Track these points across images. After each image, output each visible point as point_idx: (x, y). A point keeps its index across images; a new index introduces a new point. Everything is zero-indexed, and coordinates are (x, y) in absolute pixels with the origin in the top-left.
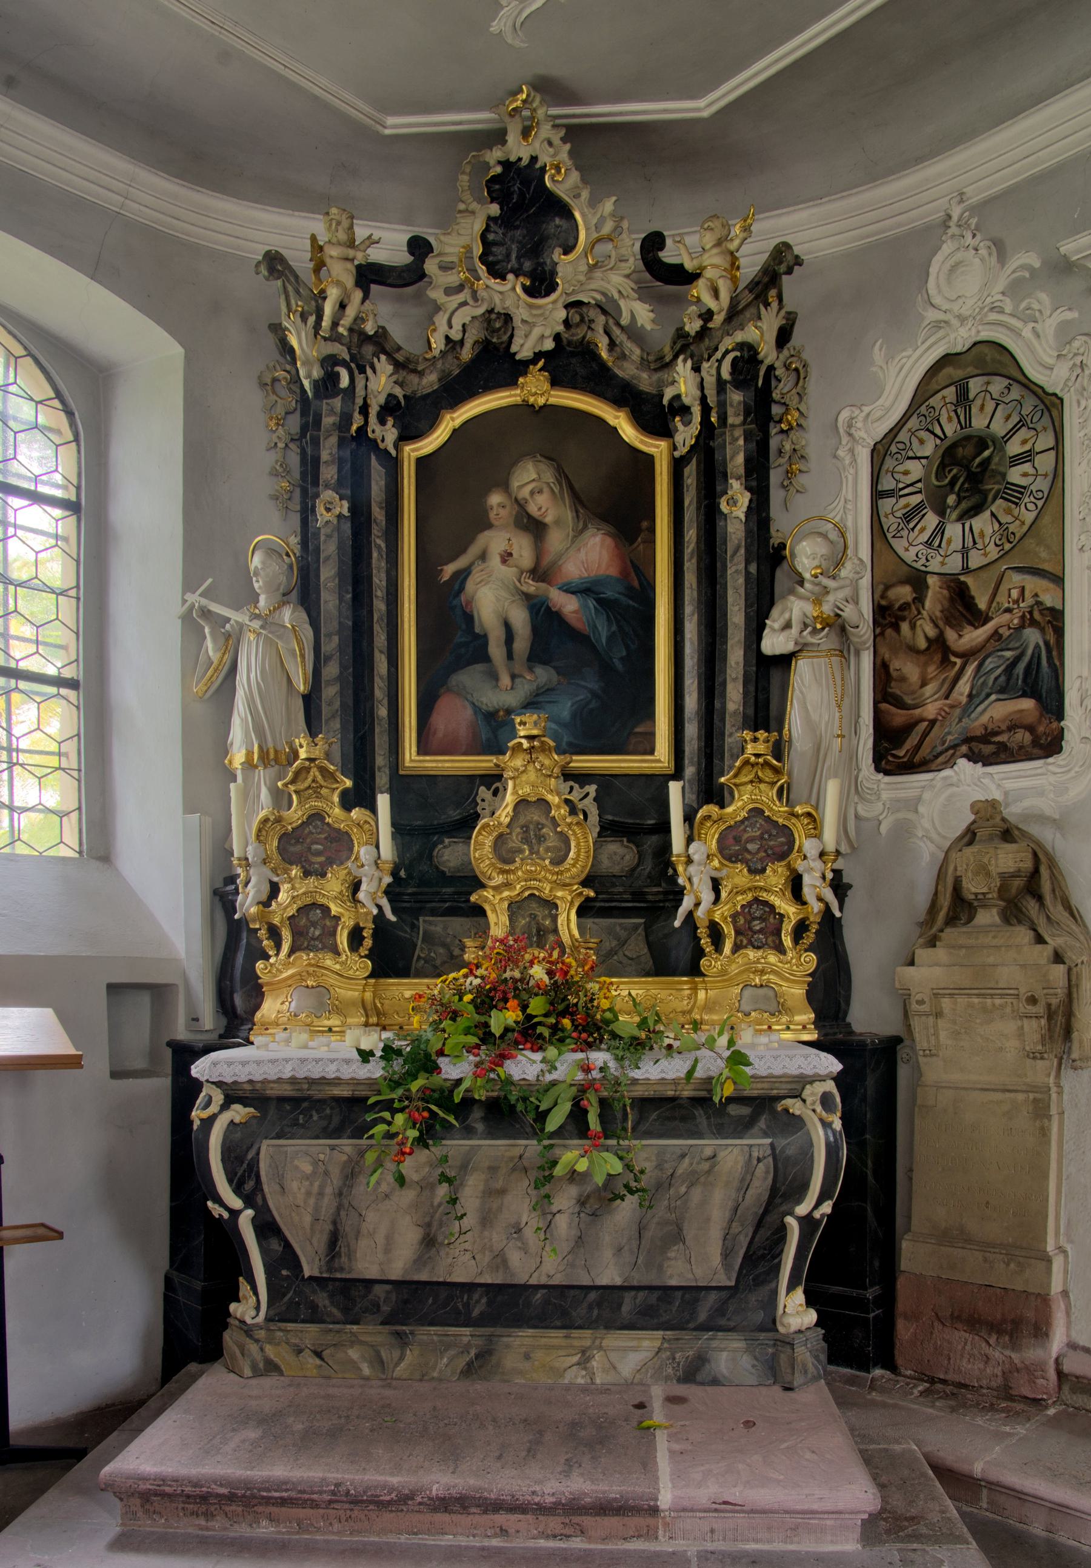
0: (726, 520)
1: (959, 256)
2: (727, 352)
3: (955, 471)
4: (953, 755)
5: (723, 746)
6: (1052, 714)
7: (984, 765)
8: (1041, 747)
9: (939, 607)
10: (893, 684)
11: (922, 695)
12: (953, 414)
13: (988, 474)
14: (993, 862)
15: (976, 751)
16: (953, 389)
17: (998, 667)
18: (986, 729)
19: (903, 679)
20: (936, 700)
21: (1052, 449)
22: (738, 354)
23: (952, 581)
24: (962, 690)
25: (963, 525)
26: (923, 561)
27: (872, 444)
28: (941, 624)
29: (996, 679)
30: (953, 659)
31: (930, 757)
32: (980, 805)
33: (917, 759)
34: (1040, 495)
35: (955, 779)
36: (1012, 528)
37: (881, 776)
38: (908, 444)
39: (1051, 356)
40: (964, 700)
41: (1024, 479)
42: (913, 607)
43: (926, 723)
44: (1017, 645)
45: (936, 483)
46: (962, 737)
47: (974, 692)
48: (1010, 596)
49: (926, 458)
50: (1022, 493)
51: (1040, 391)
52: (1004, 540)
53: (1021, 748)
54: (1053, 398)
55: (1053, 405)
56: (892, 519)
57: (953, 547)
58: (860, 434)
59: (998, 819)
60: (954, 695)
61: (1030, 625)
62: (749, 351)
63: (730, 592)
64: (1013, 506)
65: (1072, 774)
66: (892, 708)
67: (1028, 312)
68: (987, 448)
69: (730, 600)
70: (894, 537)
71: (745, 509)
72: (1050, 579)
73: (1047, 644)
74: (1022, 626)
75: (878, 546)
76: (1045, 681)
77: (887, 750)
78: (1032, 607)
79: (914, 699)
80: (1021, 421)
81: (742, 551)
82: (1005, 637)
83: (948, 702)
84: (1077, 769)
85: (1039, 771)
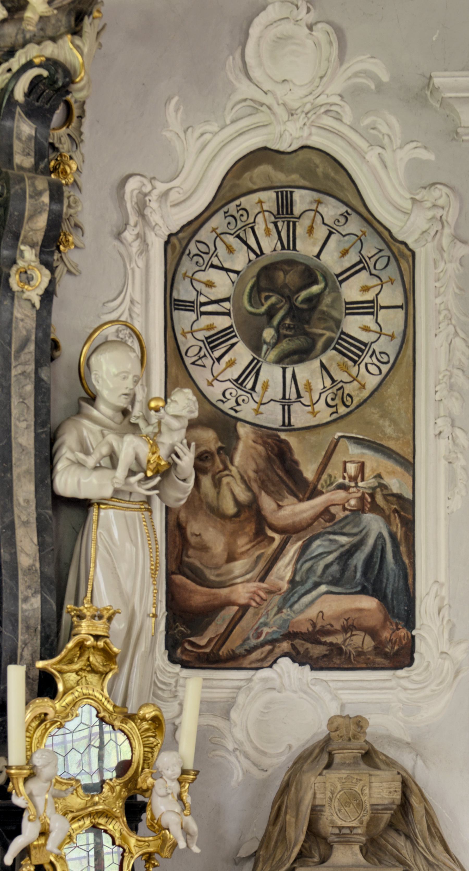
0: (13, 298)
1: (287, 28)
2: (29, 65)
3: (273, 300)
4: (271, 652)
5: (15, 616)
6: (399, 618)
7: (312, 669)
8: (386, 655)
9: (253, 466)
10: (191, 552)
11: (231, 572)
12: (271, 226)
13: (316, 315)
14: (367, 791)
15: (302, 650)
16: (272, 194)
17: (330, 553)
18: (314, 625)
19: (204, 548)
20: (248, 581)
21: (401, 307)
22: (45, 73)
23: (269, 436)
24: (281, 573)
25: (284, 370)
26: (232, 403)
27: (167, 233)
28: (255, 486)
29: (327, 567)
30: (270, 533)
31: (242, 651)
32: (340, 720)
33: (223, 651)
34: (385, 359)
35: (277, 683)
36: (348, 389)
37: (177, 668)
38: (212, 249)
39: (402, 196)
40: (285, 586)
41: (364, 333)
42: (218, 459)
43: (236, 608)
44: (355, 530)
45: (250, 309)
46: (283, 631)
47: (298, 578)
48: (345, 470)
49: (237, 272)
50: (362, 351)
51: (386, 234)
52: (338, 401)
53: (360, 654)
54: (402, 247)
55: (403, 255)
56: (192, 341)
57: (270, 394)
58: (155, 218)
59: (362, 741)
60: (272, 577)
61: (371, 511)
62: (65, 77)
63: (15, 401)
64: (350, 363)
65: (427, 691)
66: (189, 582)
67: (372, 131)
68: (316, 282)
69: (15, 412)
70: (193, 363)
71: (41, 292)
72: (396, 461)
73: (393, 536)
74: (360, 510)
75: (173, 370)
76: (391, 579)
77: (184, 635)
78: (374, 489)
79: (218, 575)
80: (360, 262)
81: (32, 347)
82: (338, 518)
83: (264, 585)
84: (433, 687)
85: (388, 684)
